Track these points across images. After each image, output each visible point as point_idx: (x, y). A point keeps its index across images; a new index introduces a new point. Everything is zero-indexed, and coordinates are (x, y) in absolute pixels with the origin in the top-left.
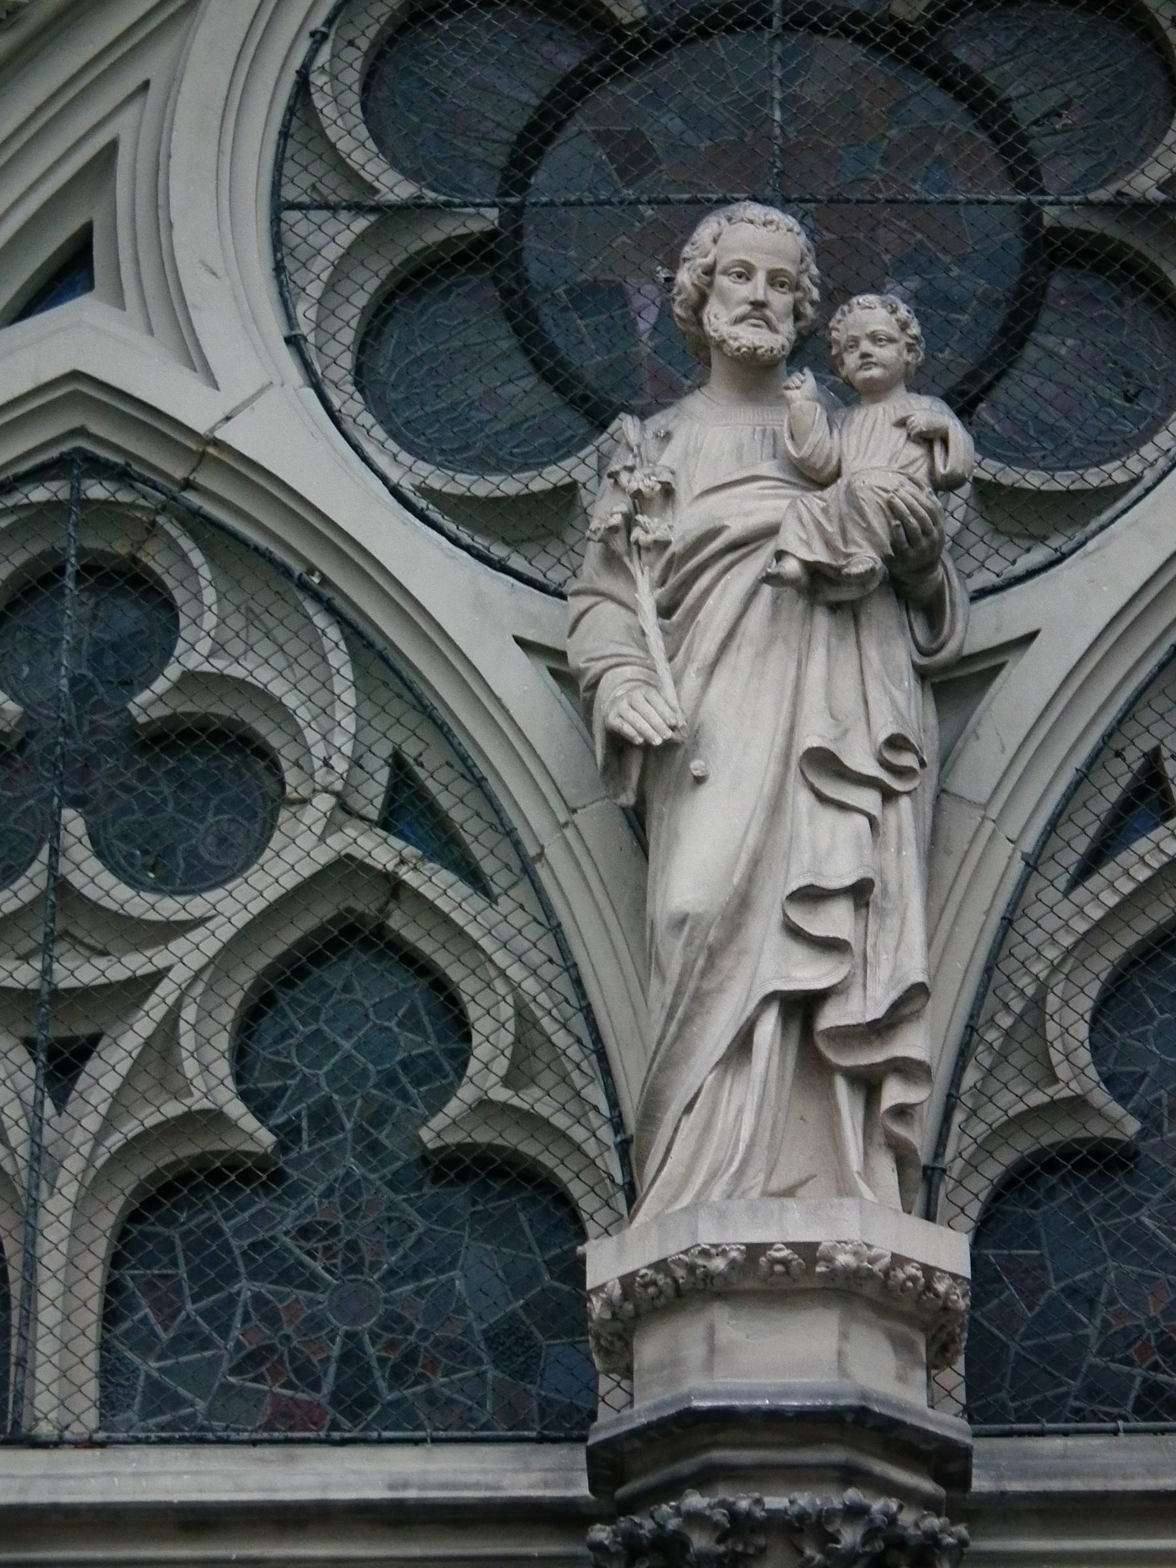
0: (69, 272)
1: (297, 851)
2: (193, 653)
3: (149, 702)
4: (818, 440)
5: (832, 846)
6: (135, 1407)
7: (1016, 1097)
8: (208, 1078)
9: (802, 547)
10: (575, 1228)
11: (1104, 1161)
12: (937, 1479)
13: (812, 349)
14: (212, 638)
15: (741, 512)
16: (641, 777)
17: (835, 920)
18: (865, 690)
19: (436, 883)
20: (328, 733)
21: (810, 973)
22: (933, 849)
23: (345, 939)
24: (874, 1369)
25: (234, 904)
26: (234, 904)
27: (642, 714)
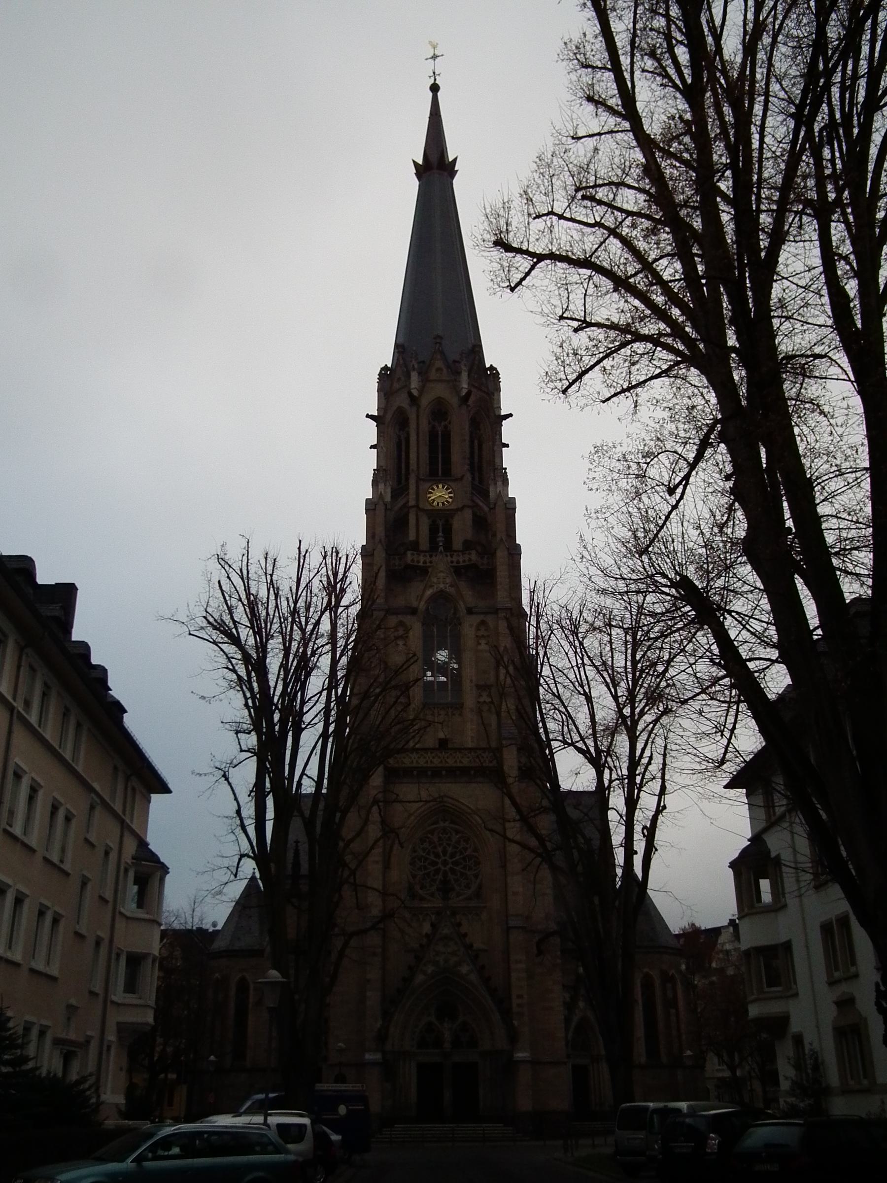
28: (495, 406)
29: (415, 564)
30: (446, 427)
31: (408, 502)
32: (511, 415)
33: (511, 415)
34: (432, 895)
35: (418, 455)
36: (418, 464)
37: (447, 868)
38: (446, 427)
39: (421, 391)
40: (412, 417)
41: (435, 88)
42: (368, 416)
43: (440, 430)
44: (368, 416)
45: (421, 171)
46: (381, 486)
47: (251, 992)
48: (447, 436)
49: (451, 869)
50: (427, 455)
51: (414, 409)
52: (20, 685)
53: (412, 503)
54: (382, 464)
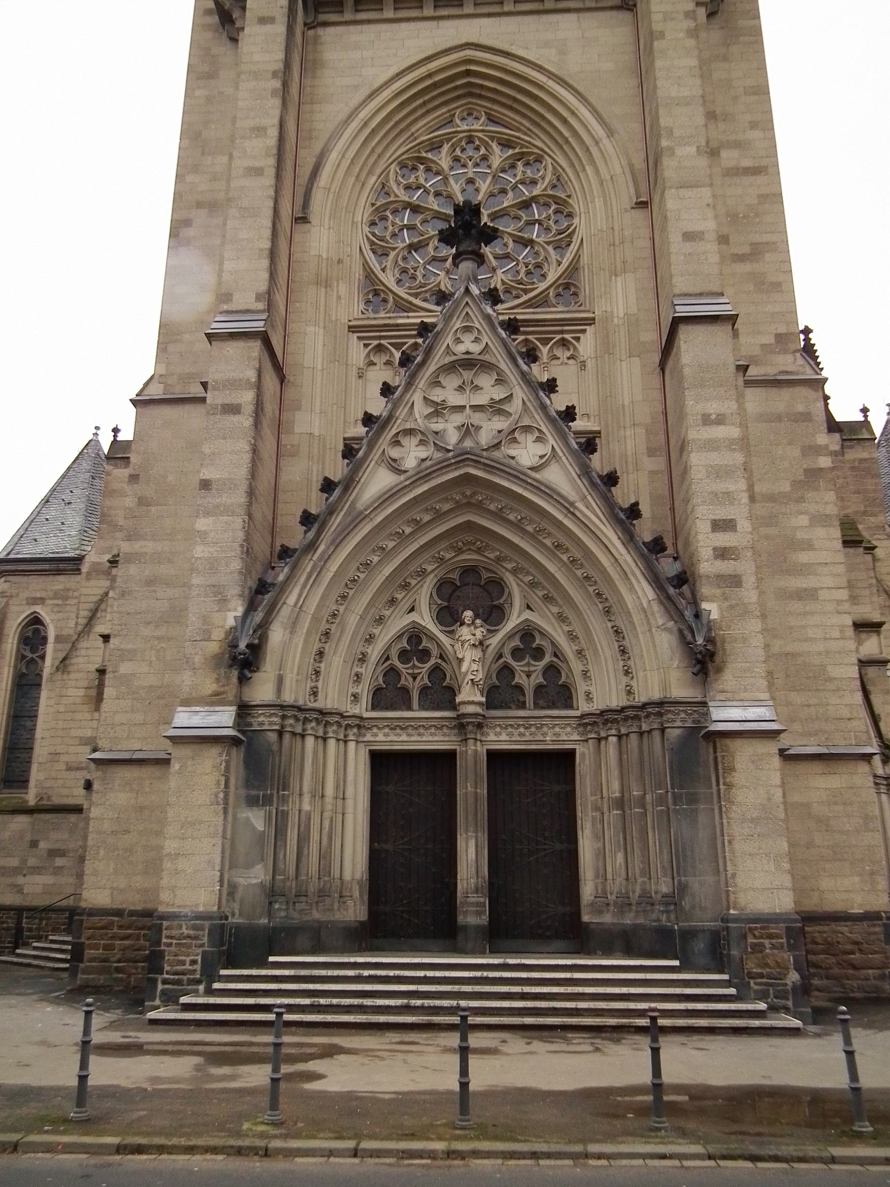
0: (412, 609)
1: (433, 661)
2: (423, 644)
3: (420, 648)
4: (474, 632)
5: (475, 667)
6: (422, 708)
7: (490, 682)
8: (426, 681)
9: (473, 642)
10: (455, 695)
11: (496, 687)
12: (307, 1092)
13: (473, 623)
14: (425, 643)
15: (468, 638)
16: (460, 661)
17: (475, 673)
18: (477, 654)
19: (443, 664)
20: (435, 652)
21: (473, 677)
22: (483, 666)
23: (436, 668)
24: (478, 709)
25: (428, 665)
26: (428, 665)
27: (460, 656)
47: (50, 647)
52: (636, 750)
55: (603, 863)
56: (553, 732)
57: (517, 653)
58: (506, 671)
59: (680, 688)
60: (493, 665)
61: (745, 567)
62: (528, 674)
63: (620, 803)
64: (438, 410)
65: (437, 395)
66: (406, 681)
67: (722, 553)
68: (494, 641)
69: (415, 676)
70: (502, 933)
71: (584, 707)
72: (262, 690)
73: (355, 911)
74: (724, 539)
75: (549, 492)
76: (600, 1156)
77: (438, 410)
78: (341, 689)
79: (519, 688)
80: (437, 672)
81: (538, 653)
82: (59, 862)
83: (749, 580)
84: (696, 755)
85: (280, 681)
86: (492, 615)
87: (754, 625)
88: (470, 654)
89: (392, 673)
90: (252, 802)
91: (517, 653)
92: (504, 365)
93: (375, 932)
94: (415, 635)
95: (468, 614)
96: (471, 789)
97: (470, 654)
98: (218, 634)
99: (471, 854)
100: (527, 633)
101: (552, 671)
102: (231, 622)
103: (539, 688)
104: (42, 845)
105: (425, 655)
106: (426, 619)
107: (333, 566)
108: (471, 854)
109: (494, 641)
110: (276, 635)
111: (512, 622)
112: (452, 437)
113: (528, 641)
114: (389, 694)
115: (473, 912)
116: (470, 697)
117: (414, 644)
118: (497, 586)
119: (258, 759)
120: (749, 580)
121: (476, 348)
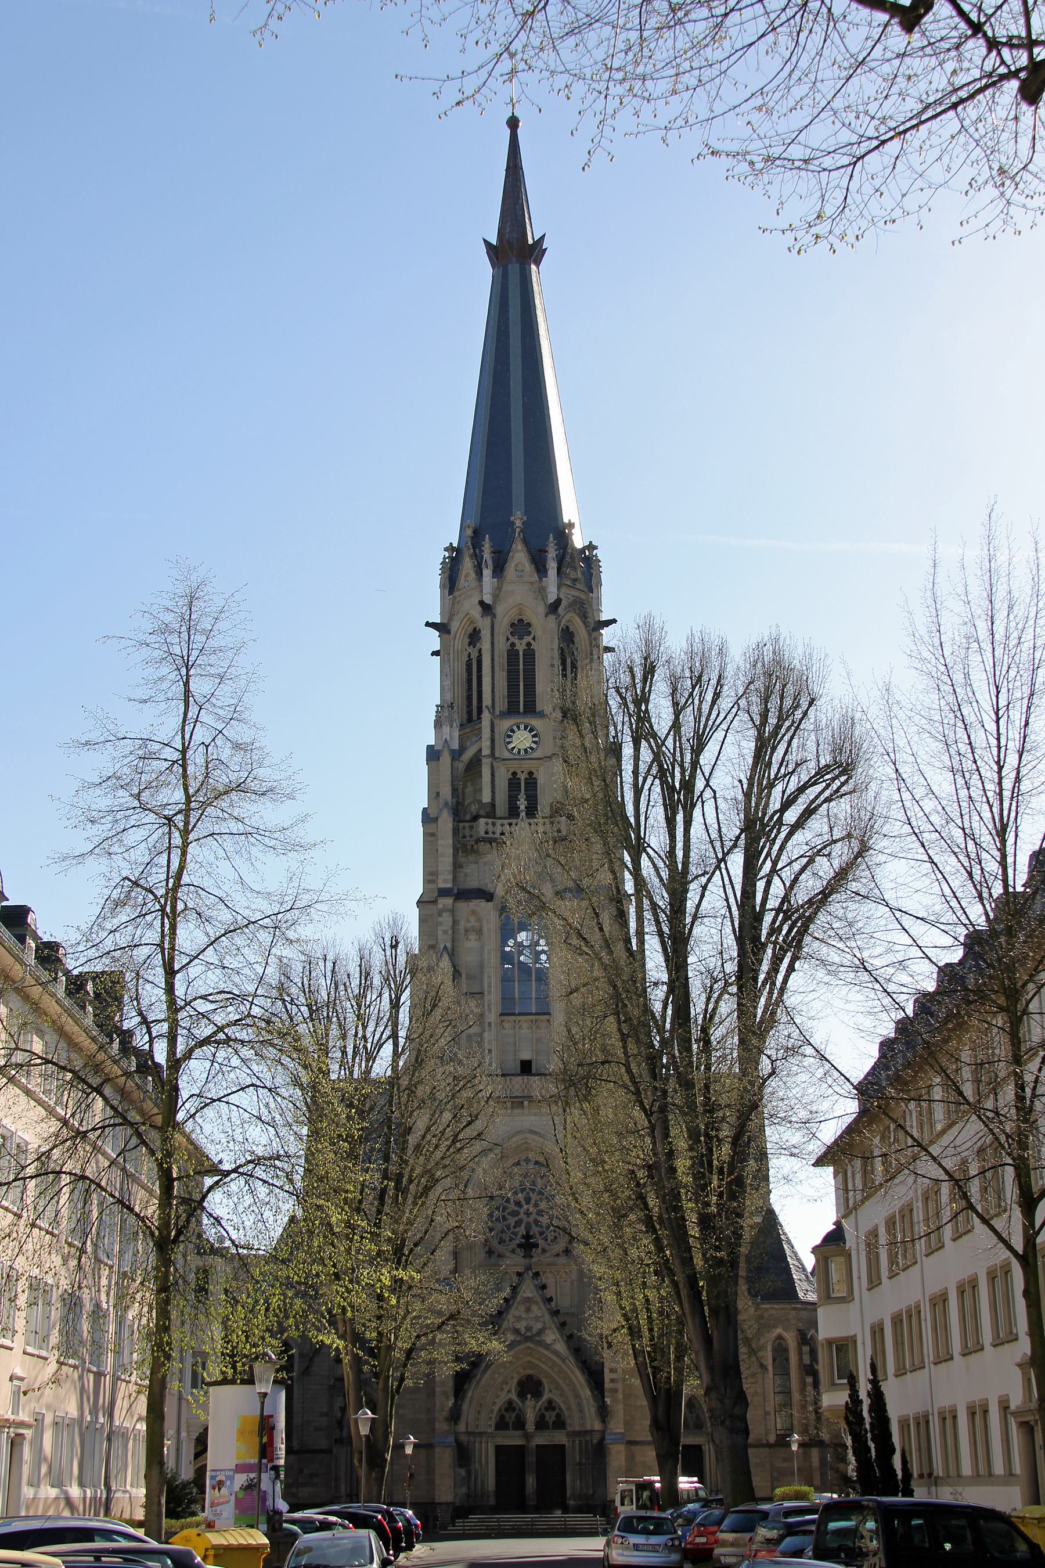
28: (595, 608)
29: (491, 835)
30: (529, 644)
31: (480, 750)
32: (614, 621)
33: (614, 621)
34: (513, 1251)
35: (493, 685)
36: (493, 700)
37: (522, 1216)
38: (529, 644)
39: (496, 596)
40: (485, 634)
41: (513, 123)
42: (428, 624)
43: (521, 647)
44: (428, 624)
45: (495, 253)
46: (446, 729)
48: (530, 655)
49: (518, 1214)
50: (506, 684)
51: (488, 621)
53: (486, 751)
54: (449, 697)
55: (572, 1481)
56: (559, 1438)
57: (546, 1409)
58: (542, 1416)
59: (598, 1426)
60: (456, 764)
61: (619, 1386)
62: (550, 1417)
63: (580, 1464)
64: (519, 1319)
65: (517, 1313)
66: (507, 1419)
67: (612, 1381)
68: (539, 1405)
69: (510, 1417)
70: (537, 1510)
71: (569, 1429)
72: (462, 1427)
73: (492, 1501)
74: (613, 1376)
75: (556, 1353)
76: (395, 1005)
77: (519, 1319)
78: (487, 1424)
79: (547, 1422)
80: (518, 1417)
81: (554, 1409)
82: (315, 1480)
83: (620, 1391)
84: (598, 1452)
85: (467, 1424)
86: (537, 1394)
87: (621, 1406)
88: (531, 1411)
89: (502, 1417)
90: (460, 1466)
91: (546, 1409)
92: (541, 1304)
93: (497, 1509)
94: (510, 1402)
95: (529, 1396)
96: (531, 1459)
97: (531, 1411)
98: (446, 1409)
99: (531, 1481)
100: (550, 1401)
101: (558, 1416)
102: (450, 1405)
103: (554, 1422)
104: (306, 1471)
105: (514, 1409)
106: (514, 1396)
107: (483, 1382)
108: (531, 1481)
109: (539, 1405)
110: (465, 1407)
111: (545, 1398)
112: (523, 1331)
113: (550, 1405)
114: (501, 1425)
115: (532, 1502)
116: (530, 1427)
117: (510, 1406)
118: (539, 1383)
119: (463, 1455)
120: (620, 1391)
121: (530, 1295)
